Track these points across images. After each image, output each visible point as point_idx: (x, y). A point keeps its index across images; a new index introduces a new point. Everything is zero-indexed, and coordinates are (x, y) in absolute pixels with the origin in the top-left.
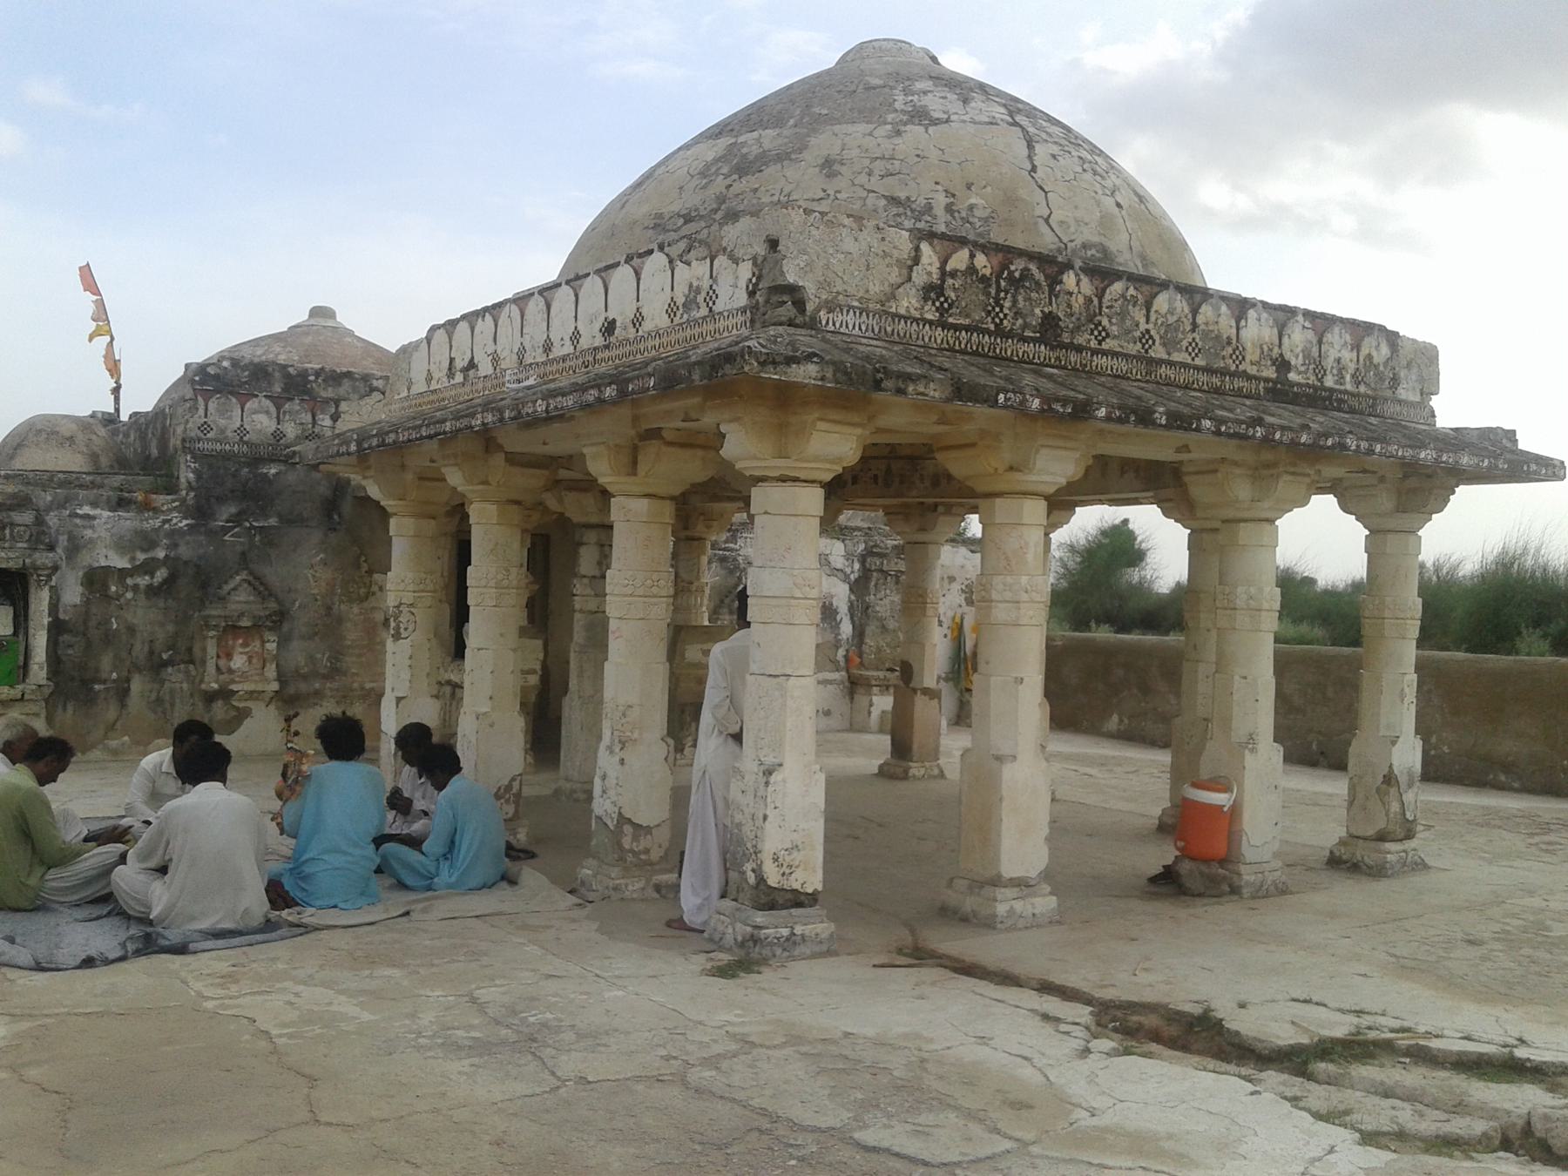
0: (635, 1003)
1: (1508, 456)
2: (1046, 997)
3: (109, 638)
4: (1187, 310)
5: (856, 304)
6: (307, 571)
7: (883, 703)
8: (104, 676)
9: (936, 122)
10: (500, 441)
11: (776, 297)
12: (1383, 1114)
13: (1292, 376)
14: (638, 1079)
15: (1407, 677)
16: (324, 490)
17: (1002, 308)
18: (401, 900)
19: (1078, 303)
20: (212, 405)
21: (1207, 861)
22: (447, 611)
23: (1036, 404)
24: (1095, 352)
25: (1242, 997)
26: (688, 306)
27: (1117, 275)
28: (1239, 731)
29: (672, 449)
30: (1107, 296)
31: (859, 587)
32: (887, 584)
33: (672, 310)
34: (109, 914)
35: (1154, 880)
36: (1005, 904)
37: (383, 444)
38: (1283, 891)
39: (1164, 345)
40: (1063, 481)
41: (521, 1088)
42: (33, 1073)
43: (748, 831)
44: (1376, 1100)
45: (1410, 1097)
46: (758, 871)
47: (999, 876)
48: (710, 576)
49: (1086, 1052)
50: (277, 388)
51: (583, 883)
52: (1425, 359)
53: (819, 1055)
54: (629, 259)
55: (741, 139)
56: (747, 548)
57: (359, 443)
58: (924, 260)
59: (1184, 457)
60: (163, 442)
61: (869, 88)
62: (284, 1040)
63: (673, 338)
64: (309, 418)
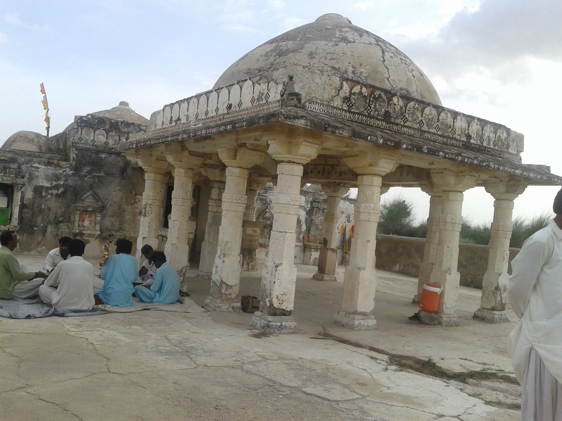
0: (225, 344)
2: (372, 352)
3: (41, 211)
4: (436, 114)
5: (319, 101)
6: (113, 192)
7: (316, 255)
8: (38, 224)
9: (350, 42)
10: (187, 146)
11: (291, 96)
12: (493, 396)
13: (472, 141)
14: (226, 367)
15: (506, 252)
16: (121, 164)
18: (141, 306)
19: (398, 108)
20: (84, 131)
21: (430, 312)
22: (162, 211)
23: (381, 141)
24: (403, 126)
25: (443, 357)
26: (259, 99)
27: (412, 99)
28: (445, 266)
30: (408, 107)
31: (310, 213)
32: (319, 211)
33: (253, 101)
34: (36, 303)
35: (411, 318)
36: (358, 321)
37: (145, 145)
38: (458, 325)
40: (388, 171)
41: (183, 366)
42: (8, 350)
43: (268, 287)
44: (490, 391)
45: (503, 391)
46: (271, 302)
47: (356, 311)
48: (257, 205)
49: (386, 369)
50: (107, 127)
51: (206, 304)
52: (519, 139)
53: (290, 364)
54: (238, 83)
56: (272, 196)
57: (137, 144)
58: (344, 88)
59: (432, 167)
60: (65, 144)
61: (327, 29)
62: (98, 346)
63: (252, 110)
64: (118, 138)
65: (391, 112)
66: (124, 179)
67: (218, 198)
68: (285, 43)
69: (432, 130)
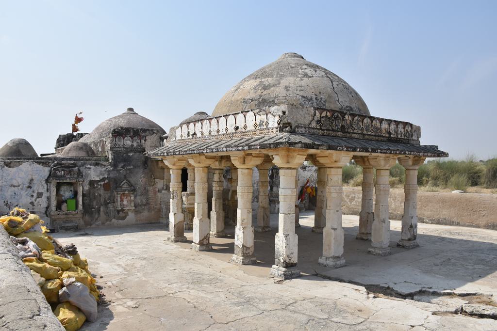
3: (95, 198)
9: (310, 77)
16: (143, 159)
20: (117, 139)
26: (260, 125)
33: (255, 126)
50: (132, 134)
55: (263, 80)
58: (317, 115)
61: (292, 68)
64: (139, 141)
66: (146, 169)
68: (266, 79)
69: (369, 133)
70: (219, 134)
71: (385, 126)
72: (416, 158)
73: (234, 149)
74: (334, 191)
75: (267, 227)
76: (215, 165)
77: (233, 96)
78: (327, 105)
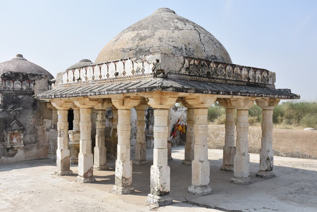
1: (290, 95)
4: (232, 69)
9: (180, 30)
16: (32, 101)
17: (200, 71)
19: (213, 69)
29: (133, 100)
30: (218, 67)
33: (133, 72)
39: (228, 76)
50: (21, 78)
52: (274, 75)
55: (140, 32)
58: (186, 63)
64: (29, 85)
65: (210, 72)
66: (35, 110)
67: (101, 120)
68: (143, 31)
69: (231, 79)
70: (101, 79)
71: (244, 72)
72: (272, 100)
73: (114, 92)
74: (201, 129)
75: (144, 160)
76: (98, 106)
77: (113, 46)
78: (194, 54)
